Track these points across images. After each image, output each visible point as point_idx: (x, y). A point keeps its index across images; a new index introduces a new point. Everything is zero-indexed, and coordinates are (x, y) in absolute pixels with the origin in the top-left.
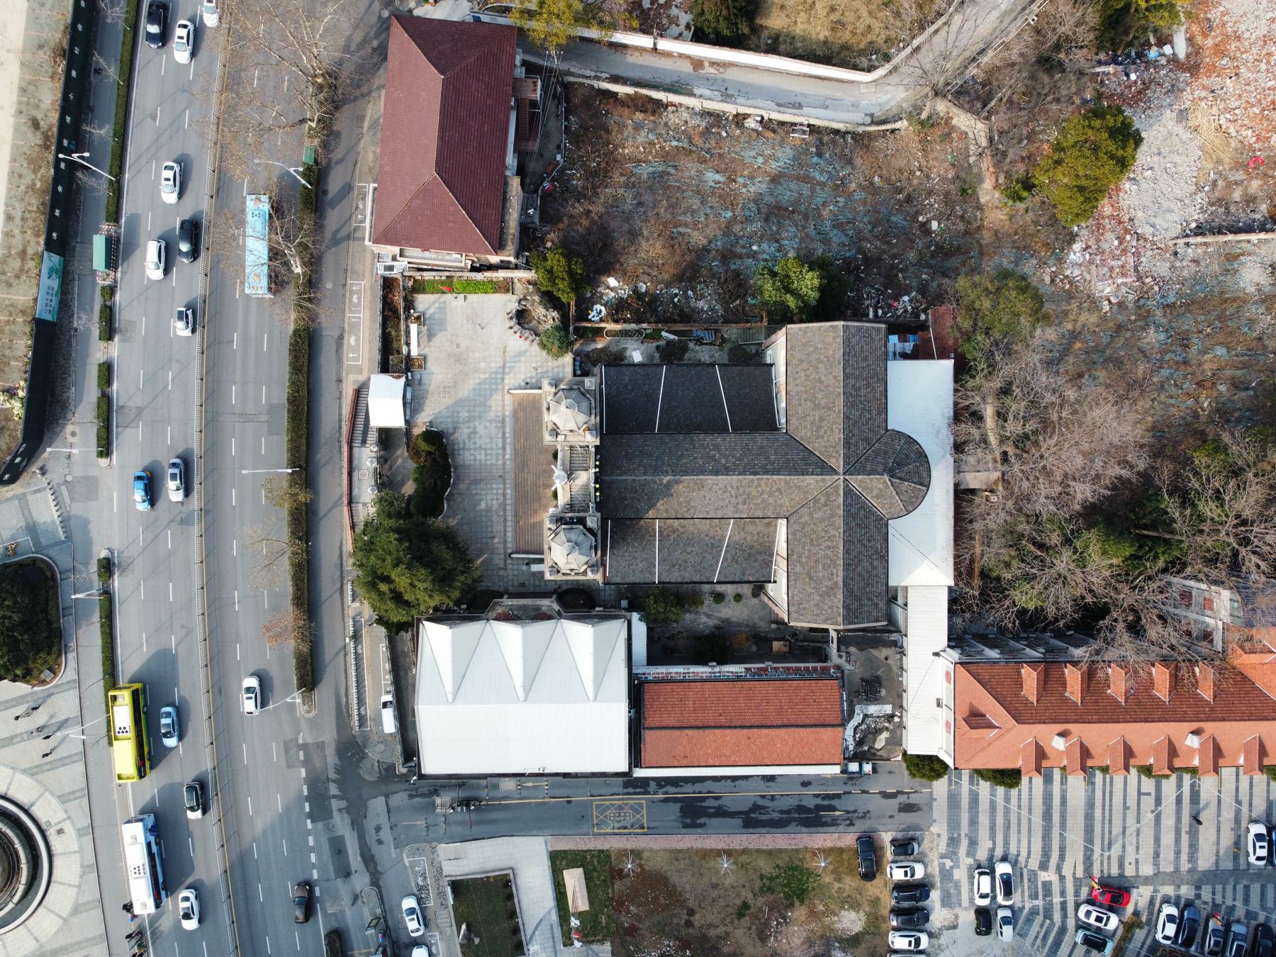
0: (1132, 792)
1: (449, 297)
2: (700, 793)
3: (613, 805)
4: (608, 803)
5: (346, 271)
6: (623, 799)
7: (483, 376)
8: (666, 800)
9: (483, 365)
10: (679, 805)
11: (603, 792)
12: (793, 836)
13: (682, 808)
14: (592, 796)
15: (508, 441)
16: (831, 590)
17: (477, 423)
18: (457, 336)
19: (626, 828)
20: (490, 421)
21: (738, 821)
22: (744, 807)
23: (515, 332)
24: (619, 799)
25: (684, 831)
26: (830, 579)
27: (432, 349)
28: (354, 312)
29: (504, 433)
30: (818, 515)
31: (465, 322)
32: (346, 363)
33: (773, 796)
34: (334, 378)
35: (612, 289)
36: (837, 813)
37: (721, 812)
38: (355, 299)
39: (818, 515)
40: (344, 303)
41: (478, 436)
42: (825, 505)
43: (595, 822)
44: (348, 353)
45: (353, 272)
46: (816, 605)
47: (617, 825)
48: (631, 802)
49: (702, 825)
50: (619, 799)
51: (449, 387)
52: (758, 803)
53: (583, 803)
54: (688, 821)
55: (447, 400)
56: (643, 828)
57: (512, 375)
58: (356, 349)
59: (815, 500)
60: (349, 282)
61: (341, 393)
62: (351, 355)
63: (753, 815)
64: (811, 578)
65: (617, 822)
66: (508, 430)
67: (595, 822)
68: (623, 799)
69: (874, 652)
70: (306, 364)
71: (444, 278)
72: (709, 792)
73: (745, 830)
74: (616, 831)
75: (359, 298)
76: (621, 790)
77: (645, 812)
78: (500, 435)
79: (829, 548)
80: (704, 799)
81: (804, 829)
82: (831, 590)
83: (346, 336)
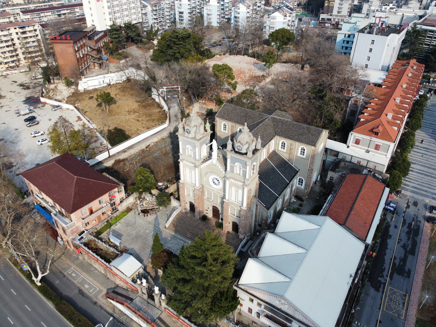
0: (419, 139)
1: (113, 227)
2: (390, 263)
3: (388, 302)
4: (386, 304)
5: (61, 272)
6: (386, 296)
7: (152, 234)
8: (391, 278)
9: (148, 231)
10: (395, 274)
11: (379, 303)
12: (422, 241)
13: (397, 273)
14: (380, 309)
15: (184, 239)
16: (308, 130)
17: (167, 245)
18: (129, 233)
19: (404, 304)
20: (171, 240)
21: (410, 257)
22: (403, 252)
23: (147, 216)
24: (385, 297)
25: (411, 279)
26: (304, 129)
27: (124, 243)
28: (77, 279)
29: (179, 239)
30: (280, 126)
31: (127, 228)
32: (91, 295)
33: (399, 239)
34: (92, 305)
35: (162, 185)
36: (413, 223)
37: (404, 260)
38: (74, 275)
39: (280, 126)
40: (70, 281)
41: (172, 248)
42: (278, 123)
43: (396, 315)
44: (89, 292)
45: (64, 269)
46: (312, 136)
47: (401, 306)
48: (388, 293)
49: (409, 271)
50: (385, 297)
51: (144, 246)
52: (402, 245)
53: (383, 315)
54: (405, 274)
55: (148, 250)
56: (405, 296)
57: (161, 225)
58: (91, 287)
59: (275, 125)
60: (65, 273)
61: (100, 306)
62: (91, 291)
63: (408, 250)
64: (301, 135)
65: (399, 304)
66: (179, 237)
67: (396, 315)
68: (386, 296)
69: (341, 166)
70: (73, 308)
71: (106, 223)
72: (391, 259)
73: (416, 256)
74: (405, 308)
75: (75, 273)
76: (380, 294)
77: (396, 290)
78: (179, 241)
79: (293, 126)
80: (394, 264)
81: (420, 236)
82: (308, 130)
83: (82, 288)
